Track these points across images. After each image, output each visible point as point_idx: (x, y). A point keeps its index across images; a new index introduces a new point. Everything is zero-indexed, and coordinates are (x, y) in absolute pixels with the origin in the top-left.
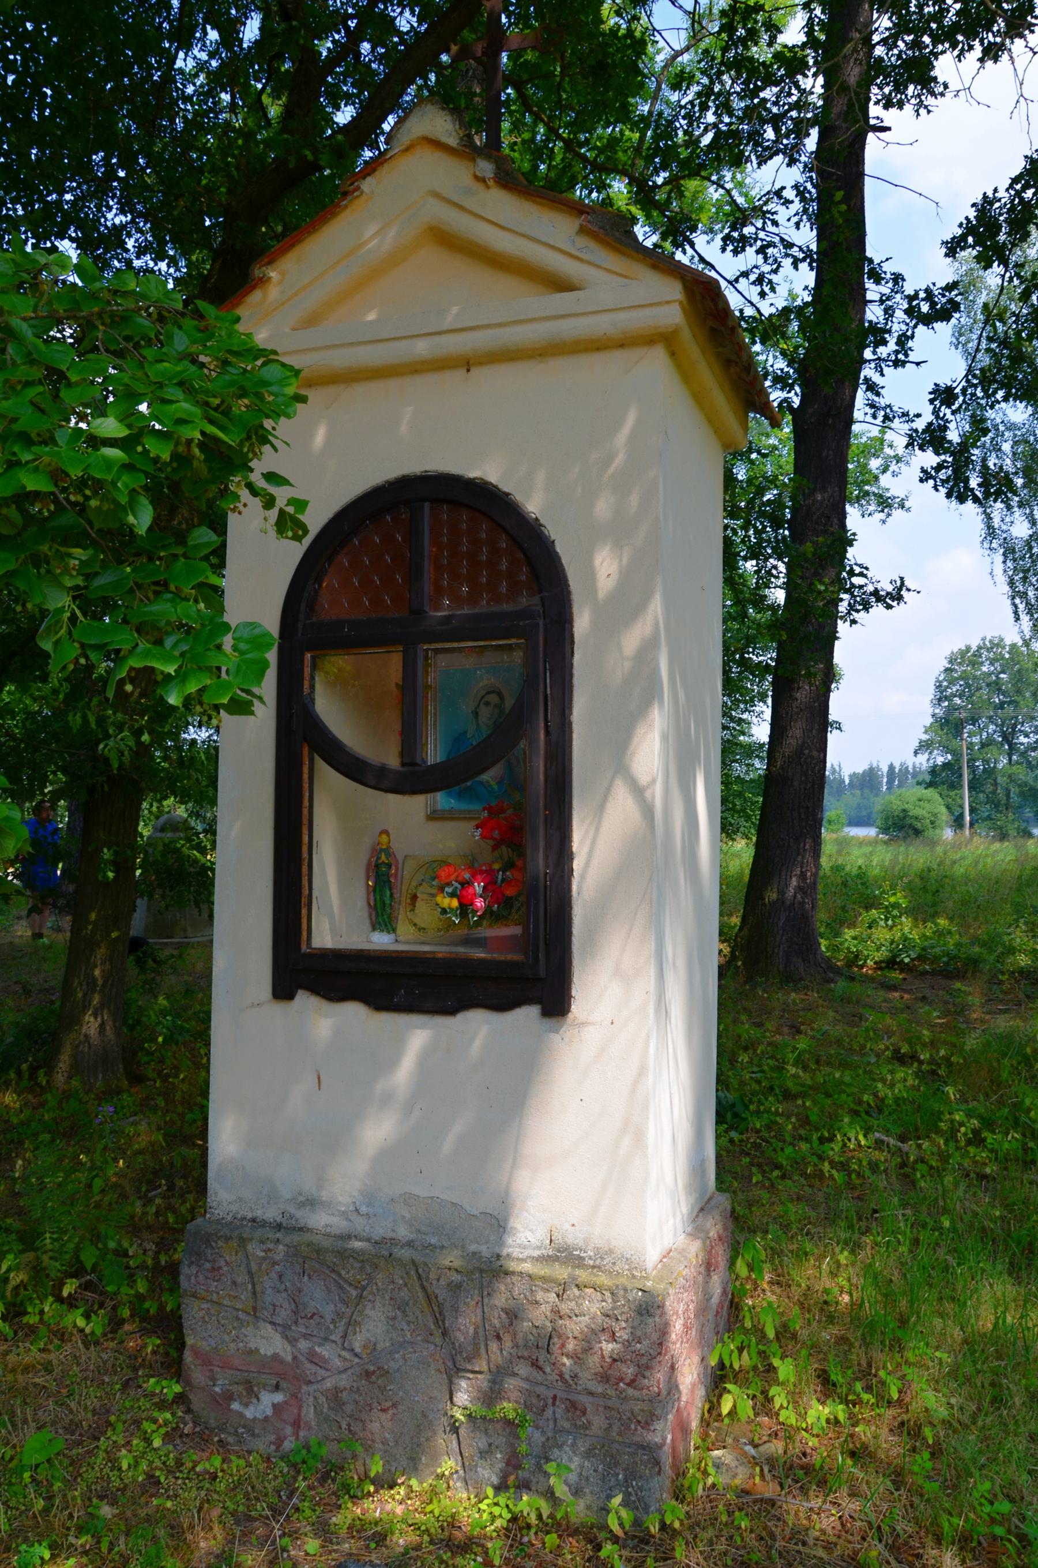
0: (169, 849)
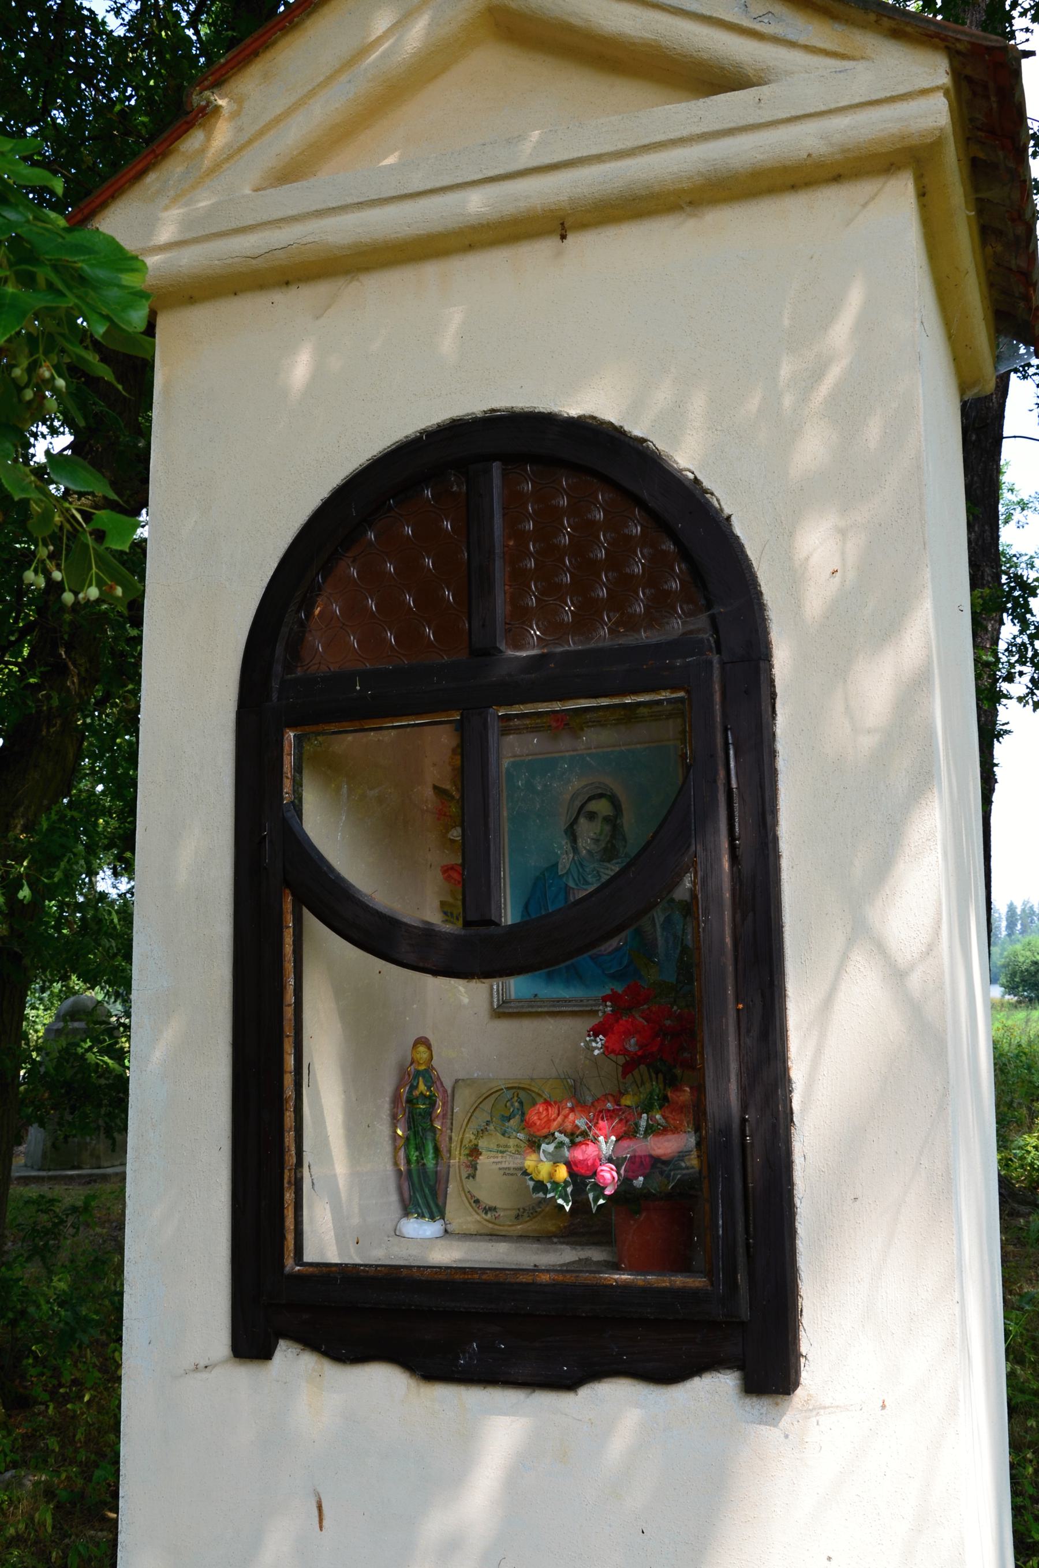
0: (69, 1056)
